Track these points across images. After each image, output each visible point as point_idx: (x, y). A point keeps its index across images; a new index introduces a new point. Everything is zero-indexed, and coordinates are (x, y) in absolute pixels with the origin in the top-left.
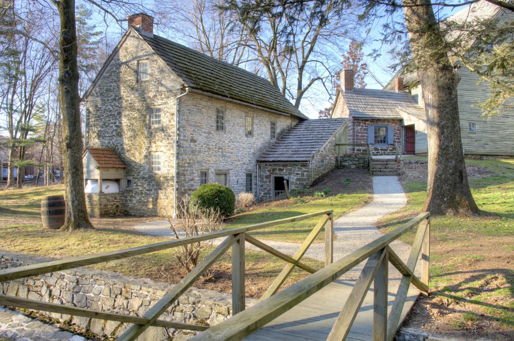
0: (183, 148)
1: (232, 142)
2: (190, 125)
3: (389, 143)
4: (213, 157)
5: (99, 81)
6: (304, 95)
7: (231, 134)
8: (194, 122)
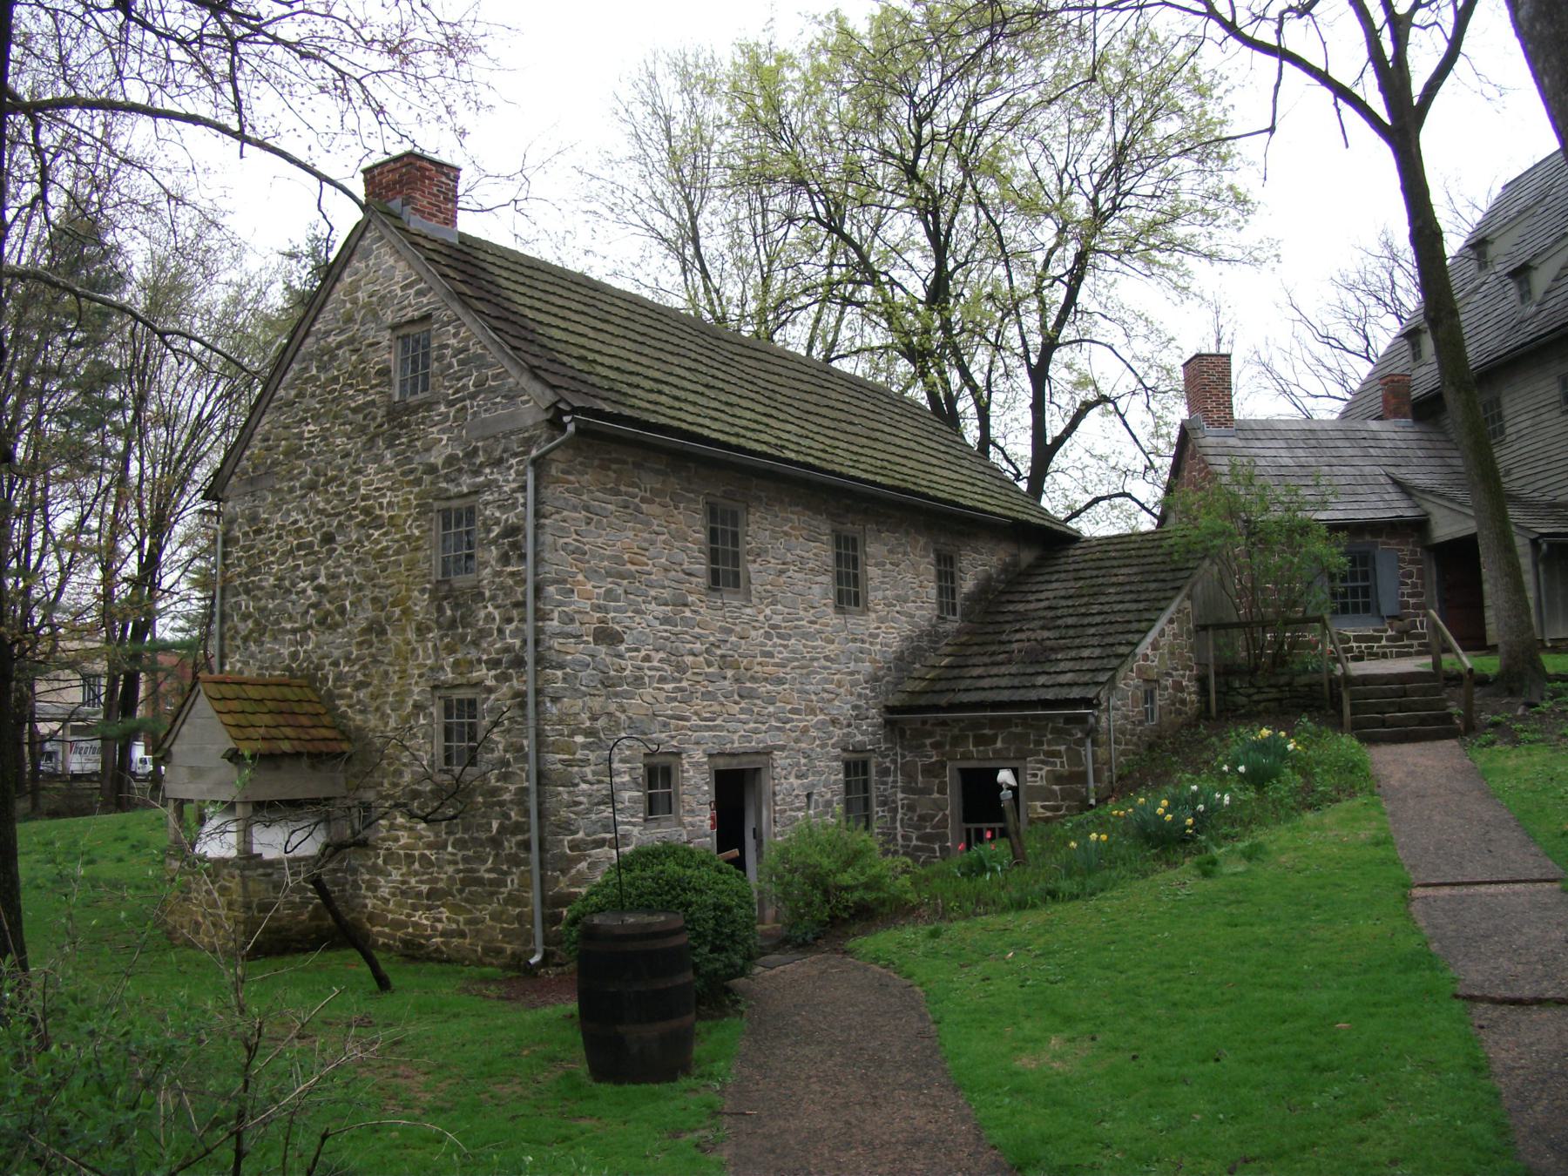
0: (561, 666)
1: (780, 636)
2: (591, 574)
3: (1385, 611)
4: (698, 704)
5: (264, 420)
6: (1058, 460)
7: (774, 603)
8: (609, 558)
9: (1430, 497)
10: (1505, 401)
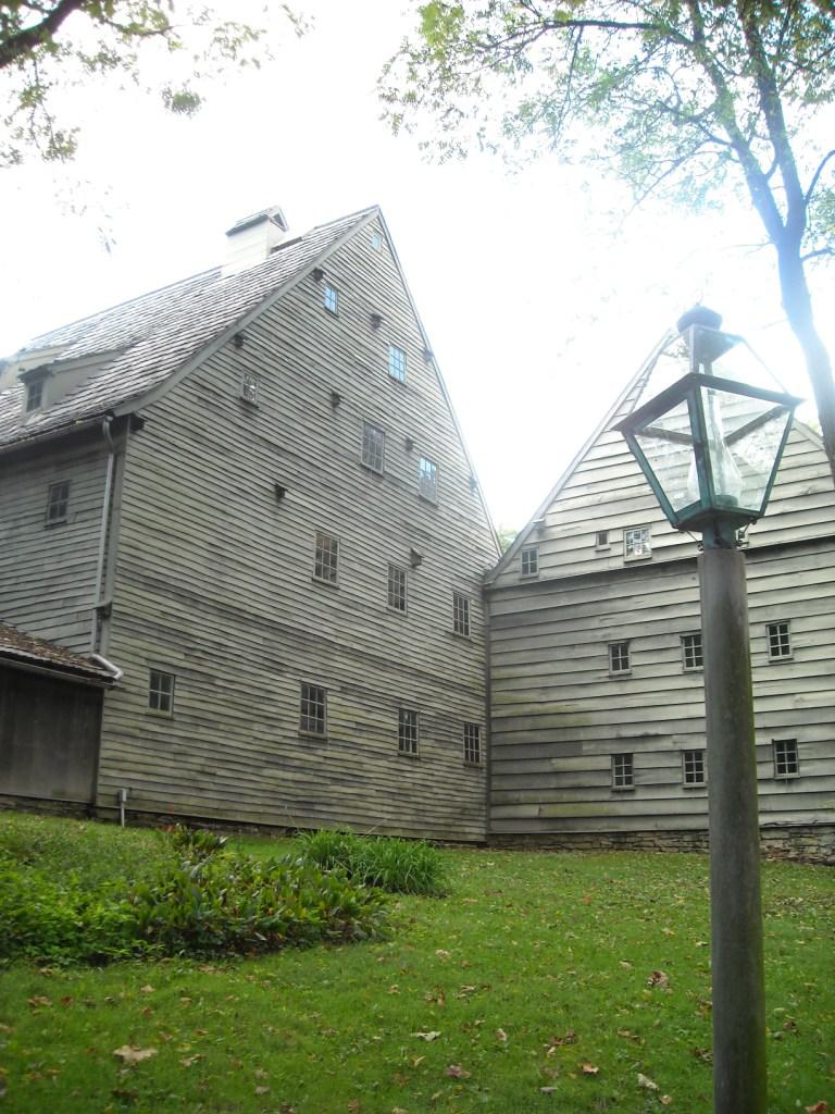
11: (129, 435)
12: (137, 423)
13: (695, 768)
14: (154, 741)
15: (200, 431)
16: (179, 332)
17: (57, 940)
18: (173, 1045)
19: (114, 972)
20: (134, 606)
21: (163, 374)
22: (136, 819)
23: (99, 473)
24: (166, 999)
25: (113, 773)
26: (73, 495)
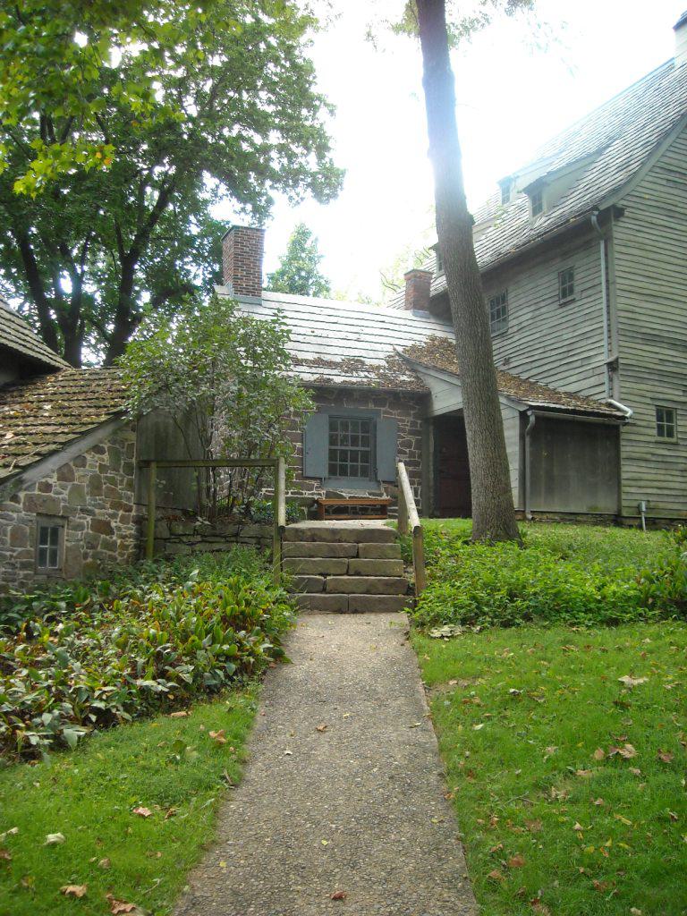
9: (432, 373)
10: (511, 296)
11: (613, 223)
12: (618, 212)
13: (53, 547)
14: (664, 463)
15: (673, 208)
16: (644, 126)
17: (583, 609)
18: (660, 676)
19: (624, 630)
20: (636, 358)
21: (634, 167)
22: (653, 524)
23: (595, 257)
24: (659, 648)
25: (633, 490)
26: (577, 277)
